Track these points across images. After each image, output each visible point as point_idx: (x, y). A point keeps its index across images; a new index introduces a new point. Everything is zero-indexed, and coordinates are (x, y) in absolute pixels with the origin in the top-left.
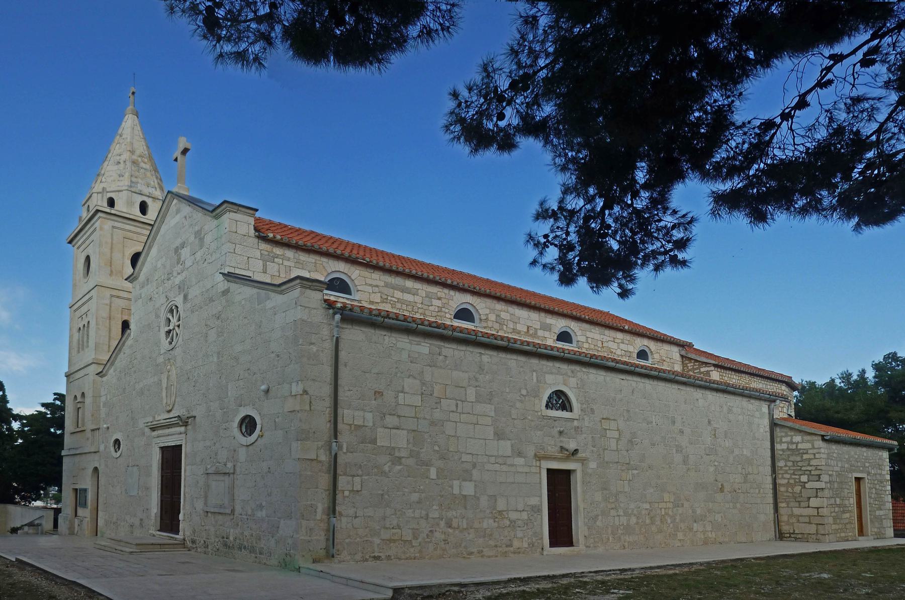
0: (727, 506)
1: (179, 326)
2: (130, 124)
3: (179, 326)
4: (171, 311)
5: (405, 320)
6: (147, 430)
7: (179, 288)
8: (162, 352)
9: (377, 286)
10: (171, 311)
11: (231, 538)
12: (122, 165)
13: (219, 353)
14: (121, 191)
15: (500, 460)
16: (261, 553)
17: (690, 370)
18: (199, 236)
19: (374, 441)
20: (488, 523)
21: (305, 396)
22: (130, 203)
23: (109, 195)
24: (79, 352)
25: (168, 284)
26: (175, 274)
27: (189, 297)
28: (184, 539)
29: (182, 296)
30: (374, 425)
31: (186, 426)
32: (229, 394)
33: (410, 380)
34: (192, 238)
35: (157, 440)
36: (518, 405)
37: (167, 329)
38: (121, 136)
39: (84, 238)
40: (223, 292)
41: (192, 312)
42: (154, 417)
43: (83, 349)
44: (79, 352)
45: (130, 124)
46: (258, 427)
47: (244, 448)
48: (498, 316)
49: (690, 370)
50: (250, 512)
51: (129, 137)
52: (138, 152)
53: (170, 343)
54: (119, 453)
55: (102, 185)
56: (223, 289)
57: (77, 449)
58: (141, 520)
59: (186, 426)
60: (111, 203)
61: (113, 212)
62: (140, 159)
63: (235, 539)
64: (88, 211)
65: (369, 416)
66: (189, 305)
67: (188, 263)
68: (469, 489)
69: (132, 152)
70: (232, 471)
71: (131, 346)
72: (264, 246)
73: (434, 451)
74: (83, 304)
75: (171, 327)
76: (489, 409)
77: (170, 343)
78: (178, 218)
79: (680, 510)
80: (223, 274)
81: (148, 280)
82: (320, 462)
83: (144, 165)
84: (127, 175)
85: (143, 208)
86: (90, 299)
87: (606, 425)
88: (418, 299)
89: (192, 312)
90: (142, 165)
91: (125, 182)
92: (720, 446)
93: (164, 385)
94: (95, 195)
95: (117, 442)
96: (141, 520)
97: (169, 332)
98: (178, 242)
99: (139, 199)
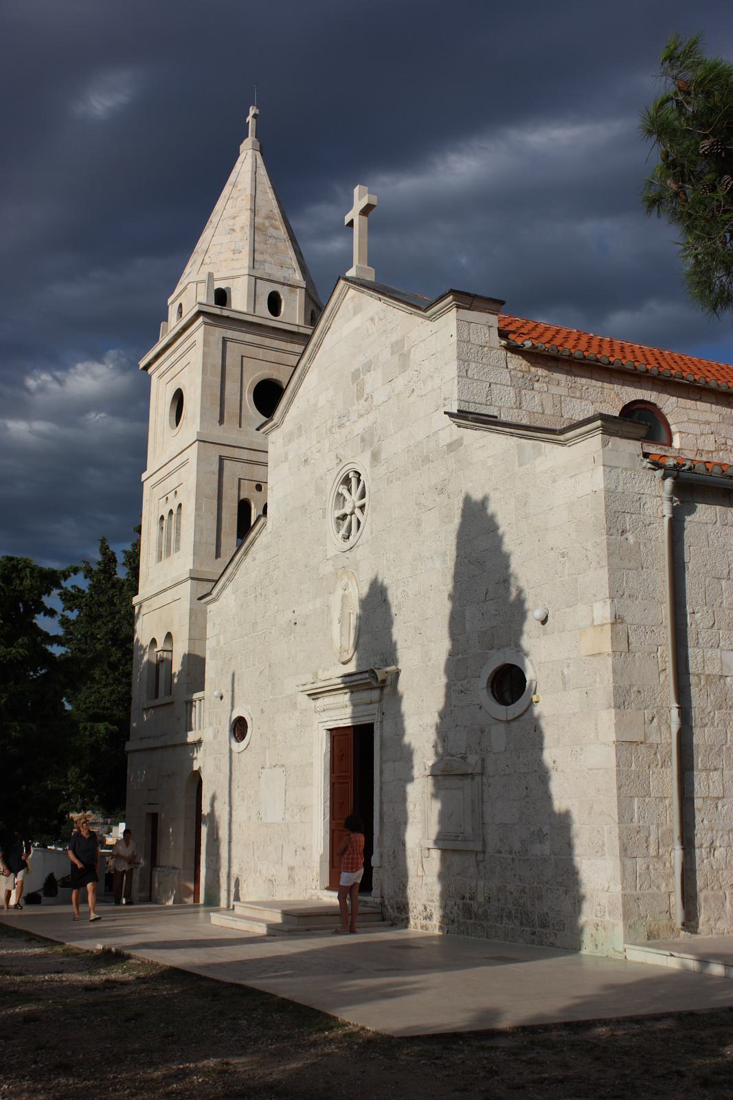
1: (362, 508)
4: (347, 481)
6: (303, 699)
7: (363, 440)
8: (330, 554)
9: (708, 423)
10: (347, 481)
11: (481, 899)
14: (238, 277)
16: (543, 926)
18: (402, 354)
22: (254, 296)
26: (354, 417)
27: (383, 456)
28: (382, 904)
29: (367, 456)
32: (468, 626)
37: (339, 513)
39: (173, 358)
40: (449, 445)
42: (316, 674)
43: (168, 553)
44: (160, 558)
47: (502, 727)
50: (517, 846)
56: (449, 441)
58: (292, 869)
61: (225, 313)
62: (267, 224)
64: (180, 313)
67: (379, 398)
70: (478, 770)
72: (517, 362)
74: (169, 474)
75: (348, 511)
78: (357, 321)
80: (451, 415)
81: (300, 428)
82: (651, 746)
89: (389, 482)
90: (271, 231)
94: (192, 287)
96: (292, 869)
99: (265, 289)
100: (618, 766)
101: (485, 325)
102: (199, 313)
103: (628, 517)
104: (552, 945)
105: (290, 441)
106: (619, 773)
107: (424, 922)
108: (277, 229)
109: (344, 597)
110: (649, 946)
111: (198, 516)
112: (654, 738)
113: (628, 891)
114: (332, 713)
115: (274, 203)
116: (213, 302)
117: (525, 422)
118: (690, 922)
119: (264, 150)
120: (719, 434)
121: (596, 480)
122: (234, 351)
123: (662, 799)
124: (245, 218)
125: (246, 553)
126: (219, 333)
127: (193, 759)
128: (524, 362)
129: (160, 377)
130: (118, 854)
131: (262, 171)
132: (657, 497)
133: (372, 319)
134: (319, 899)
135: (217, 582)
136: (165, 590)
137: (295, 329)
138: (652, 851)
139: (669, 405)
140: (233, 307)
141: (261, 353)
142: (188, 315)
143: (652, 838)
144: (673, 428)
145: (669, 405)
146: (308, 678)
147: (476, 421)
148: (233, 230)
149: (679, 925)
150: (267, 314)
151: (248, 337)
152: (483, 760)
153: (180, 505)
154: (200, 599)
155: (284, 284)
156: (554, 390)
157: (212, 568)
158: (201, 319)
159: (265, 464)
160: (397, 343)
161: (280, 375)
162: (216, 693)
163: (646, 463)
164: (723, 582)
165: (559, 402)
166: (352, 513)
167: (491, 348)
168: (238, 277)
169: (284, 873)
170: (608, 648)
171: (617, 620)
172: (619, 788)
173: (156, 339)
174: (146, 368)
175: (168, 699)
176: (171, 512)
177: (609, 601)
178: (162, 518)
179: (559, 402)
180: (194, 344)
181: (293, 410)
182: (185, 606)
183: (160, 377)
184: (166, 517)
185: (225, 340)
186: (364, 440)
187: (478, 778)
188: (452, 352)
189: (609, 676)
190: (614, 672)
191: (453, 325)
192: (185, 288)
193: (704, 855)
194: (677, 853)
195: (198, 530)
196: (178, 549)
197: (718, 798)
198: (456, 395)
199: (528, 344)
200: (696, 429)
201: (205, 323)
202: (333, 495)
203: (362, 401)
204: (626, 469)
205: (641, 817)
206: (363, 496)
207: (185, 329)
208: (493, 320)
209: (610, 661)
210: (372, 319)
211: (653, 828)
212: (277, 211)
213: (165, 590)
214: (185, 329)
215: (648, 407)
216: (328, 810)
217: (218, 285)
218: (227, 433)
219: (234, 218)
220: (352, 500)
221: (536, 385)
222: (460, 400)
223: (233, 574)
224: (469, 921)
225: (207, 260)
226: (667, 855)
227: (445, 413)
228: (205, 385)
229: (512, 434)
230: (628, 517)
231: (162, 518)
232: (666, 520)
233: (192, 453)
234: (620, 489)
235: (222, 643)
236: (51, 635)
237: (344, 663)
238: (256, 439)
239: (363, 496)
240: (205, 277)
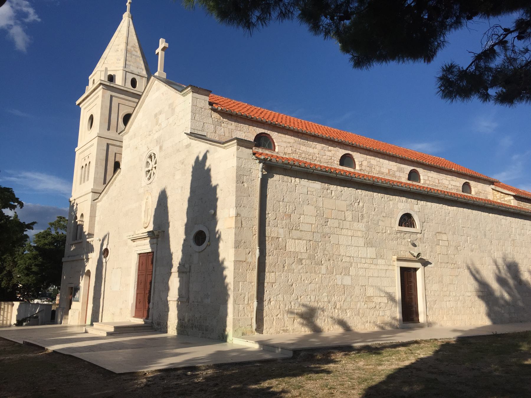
1: (155, 168)
2: (126, 23)
4: (150, 157)
7: (157, 141)
10: (150, 157)
13: (182, 187)
14: (119, 70)
16: (206, 330)
17: (498, 199)
20: (361, 305)
24: (81, 184)
26: (154, 132)
27: (164, 148)
28: (152, 323)
29: (158, 147)
31: (157, 238)
35: (136, 249)
37: (147, 169)
40: (186, 146)
42: (135, 232)
43: (84, 182)
44: (81, 184)
45: (126, 23)
46: (207, 239)
49: (498, 199)
53: (149, 179)
56: (186, 144)
57: (74, 256)
58: (121, 309)
59: (157, 238)
61: (112, 85)
62: (132, 49)
63: (189, 321)
64: (94, 83)
65: (281, 231)
68: (347, 281)
72: (215, 115)
75: (150, 168)
76: (361, 226)
77: (149, 179)
80: (187, 134)
81: (135, 135)
85: (134, 83)
87: (439, 237)
88: (316, 151)
89: (165, 158)
93: (143, 209)
94: (99, 73)
96: (121, 309)
99: (130, 77)
100: (234, 269)
101: (203, 100)
102: (100, 84)
103: (245, 177)
104: (209, 338)
105: (131, 139)
106: (234, 272)
108: (136, 52)
109: (147, 202)
110: (243, 338)
111: (96, 167)
112: (249, 260)
113: (235, 317)
114: (139, 247)
115: (136, 41)
116: (107, 80)
117: (217, 139)
118: (260, 328)
119: (133, 18)
120: (293, 147)
121: (233, 162)
122: (115, 101)
123: (251, 283)
124: (123, 46)
126: (109, 93)
127: (85, 266)
128: (218, 115)
129: (85, 109)
130: (116, 328)
131: (132, 27)
132: (257, 170)
133: (163, 94)
134: (130, 321)
135: (101, 194)
136: (81, 196)
138: (246, 302)
139: (275, 136)
140: (116, 83)
141: (127, 103)
142: (97, 83)
143: (246, 298)
144: (276, 144)
146: (132, 233)
147: (195, 137)
148: (118, 51)
149: (254, 330)
150: (131, 87)
152: (190, 266)
153: (90, 162)
154: (94, 200)
155: (138, 75)
156: (229, 127)
157: (100, 188)
158: (101, 86)
159: (122, 147)
162: (97, 239)
163: (254, 157)
164: (281, 203)
165: (231, 132)
166: (152, 170)
167: (205, 109)
168: (119, 70)
170: (233, 225)
171: (238, 215)
172: (234, 278)
174: (79, 104)
175: (80, 241)
176: (86, 165)
177: (235, 208)
178: (83, 167)
179: (231, 132)
180: (98, 97)
181: (133, 127)
182: (89, 203)
184: (84, 167)
185: (111, 97)
186: (158, 142)
187: (188, 274)
188: (189, 110)
189: (233, 236)
190: (235, 234)
191: (190, 100)
192: (96, 73)
193: (266, 304)
194: (255, 303)
195: (96, 173)
196: (88, 180)
198: (190, 127)
199: (220, 108)
200: (285, 145)
201: (103, 89)
202: (145, 162)
203: (157, 126)
204: (246, 159)
205: (242, 289)
206: (156, 163)
207: (94, 90)
208: (207, 98)
209: (234, 230)
210: (163, 94)
211: (247, 293)
212: (137, 44)
213: (81, 196)
214: (94, 90)
215: (267, 135)
216: (136, 286)
217: (109, 73)
218: (112, 134)
219: (118, 45)
221: (223, 125)
222: (191, 128)
223: (107, 191)
225: (106, 62)
226: (252, 304)
228: (102, 114)
229: (210, 144)
230: (245, 177)
231: (83, 167)
232: (260, 179)
233: (95, 141)
234: (243, 166)
237: (145, 228)
238: (118, 137)
239: (156, 163)
240: (104, 69)
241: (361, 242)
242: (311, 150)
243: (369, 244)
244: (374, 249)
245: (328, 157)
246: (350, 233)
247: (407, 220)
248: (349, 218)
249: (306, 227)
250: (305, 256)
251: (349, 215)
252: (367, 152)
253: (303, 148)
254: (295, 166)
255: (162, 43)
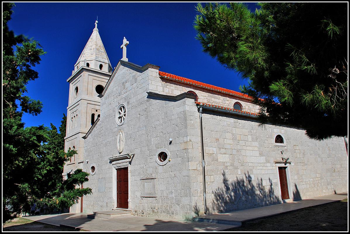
0: (337, 177)
1: (125, 115)
2: (95, 36)
3: (125, 115)
5: (225, 109)
9: (205, 96)
12: (92, 51)
15: (262, 165)
19: (217, 160)
21: (190, 142)
22: (96, 65)
23: (87, 62)
25: (119, 98)
26: (122, 93)
27: (130, 103)
30: (217, 153)
33: (228, 133)
34: (131, 78)
36: (266, 141)
37: (119, 116)
38: (92, 39)
41: (132, 109)
45: (95, 36)
48: (249, 107)
51: (95, 39)
52: (99, 45)
54: (94, 173)
55: (84, 58)
60: (88, 65)
61: (89, 69)
65: (215, 149)
66: (130, 106)
69: (96, 45)
71: (100, 124)
73: (239, 162)
74: (74, 107)
79: (323, 180)
82: (198, 170)
83: (101, 50)
84: (94, 54)
86: (78, 105)
88: (220, 101)
89: (132, 109)
91: (94, 57)
92: (331, 154)
95: (93, 168)
97: (120, 118)
98: (124, 80)
107: (142, 215)
109: (120, 137)
125: (94, 126)
129: (72, 84)
135: (87, 134)
137: (106, 73)
139: (197, 92)
141: (97, 79)
145: (197, 92)
151: (94, 75)
156: (171, 88)
160: (134, 76)
161: (104, 85)
165: (172, 90)
169: (105, 204)
173: (71, 75)
183: (72, 84)
197: (213, 182)
220: (122, 113)
224: (153, 214)
227: (147, 92)
235: (88, 148)
236: (304, 132)
241: (257, 153)
242: (217, 100)
243: (261, 154)
244: (264, 157)
245: (228, 103)
246: (251, 148)
247: (279, 139)
248: (250, 139)
249: (228, 147)
250: (228, 164)
251: (250, 138)
252: (247, 101)
253: (213, 99)
254: (220, 109)
255: (125, 41)
